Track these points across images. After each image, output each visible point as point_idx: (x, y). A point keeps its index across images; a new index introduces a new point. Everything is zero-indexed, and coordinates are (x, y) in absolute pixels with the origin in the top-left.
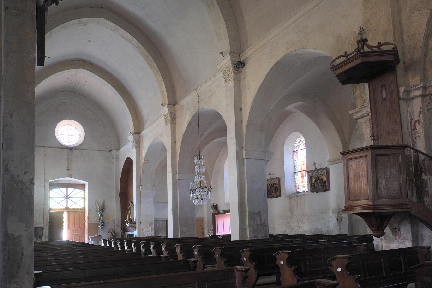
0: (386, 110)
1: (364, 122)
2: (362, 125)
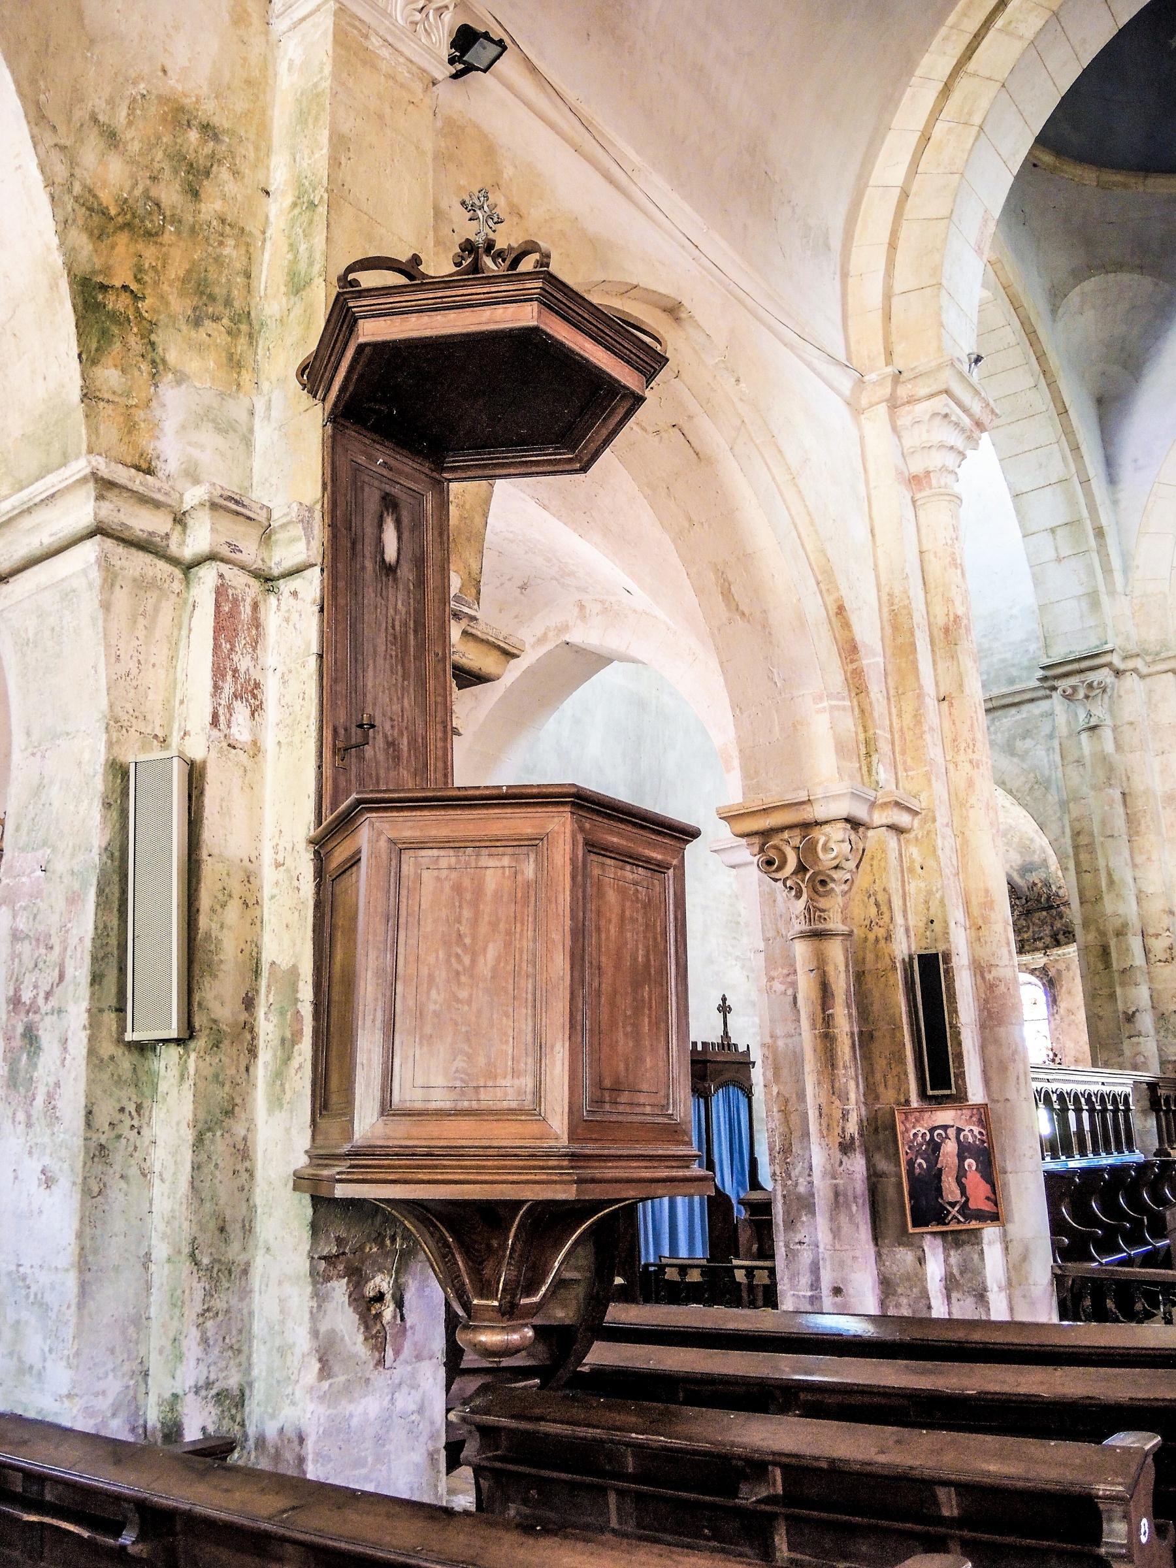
0: (393, 627)
1: (135, 580)
2: (117, 588)
